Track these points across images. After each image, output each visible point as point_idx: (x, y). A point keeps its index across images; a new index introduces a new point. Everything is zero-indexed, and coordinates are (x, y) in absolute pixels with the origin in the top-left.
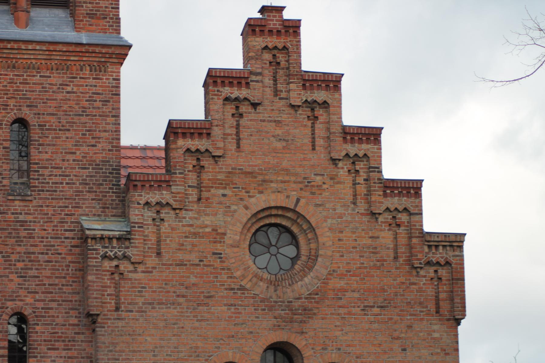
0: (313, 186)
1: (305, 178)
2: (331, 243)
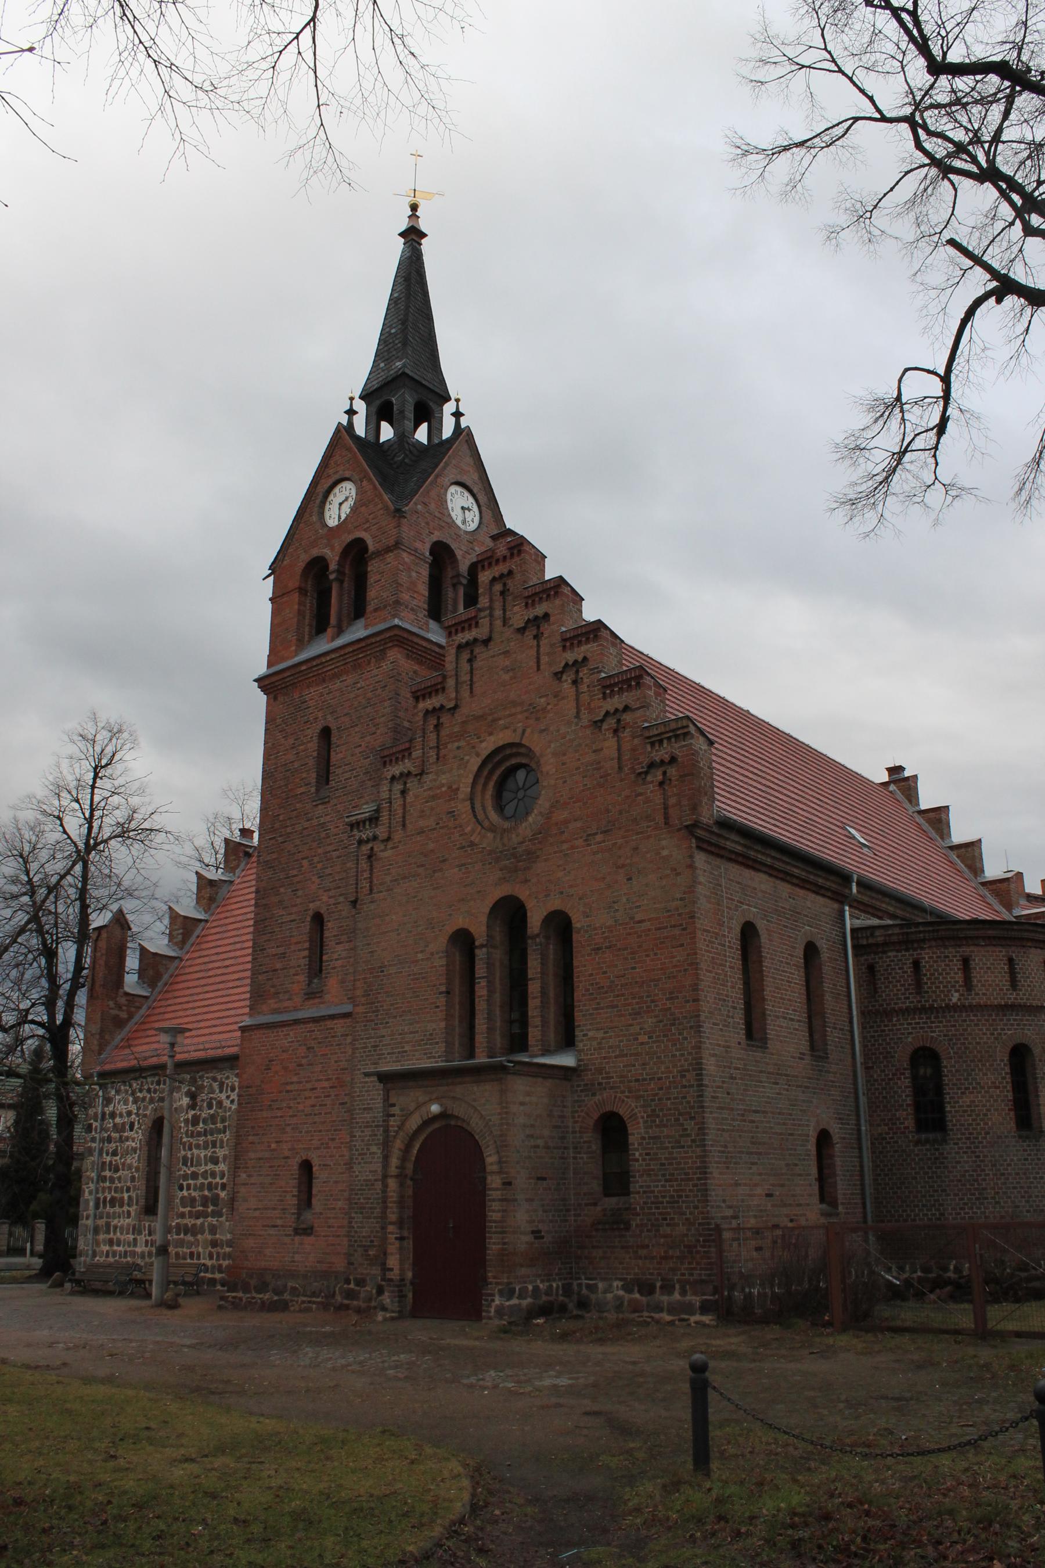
1: (530, 705)
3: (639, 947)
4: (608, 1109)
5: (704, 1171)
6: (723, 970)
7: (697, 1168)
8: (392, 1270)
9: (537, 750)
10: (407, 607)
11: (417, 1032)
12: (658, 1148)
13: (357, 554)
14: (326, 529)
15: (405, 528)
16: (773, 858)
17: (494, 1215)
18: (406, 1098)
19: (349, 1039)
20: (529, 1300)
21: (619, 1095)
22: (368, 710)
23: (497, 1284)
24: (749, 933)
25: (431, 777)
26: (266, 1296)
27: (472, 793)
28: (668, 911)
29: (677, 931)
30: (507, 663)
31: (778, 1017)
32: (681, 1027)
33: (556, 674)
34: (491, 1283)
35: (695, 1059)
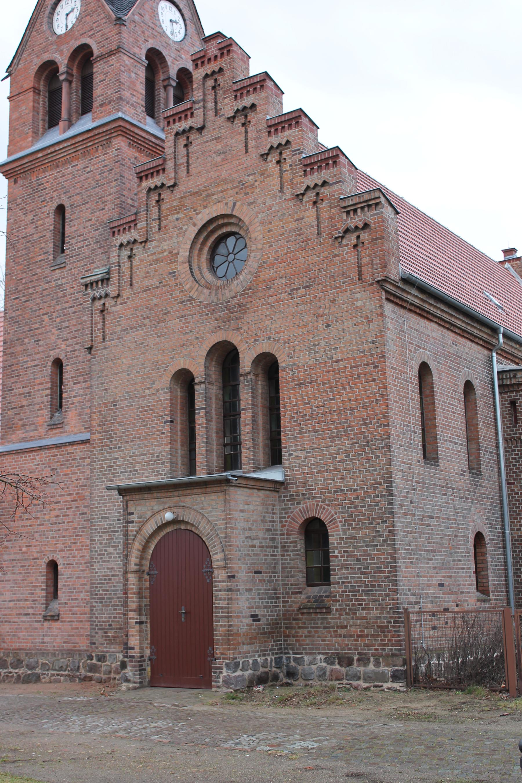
0: (247, 187)
1: (240, 182)
2: (262, 236)
3: (337, 382)
4: (312, 515)
5: (394, 567)
6: (406, 401)
7: (389, 563)
8: (133, 648)
9: (246, 220)
10: (128, 103)
11: (146, 454)
12: (355, 547)
13: (83, 57)
14: (55, 37)
15: (125, 35)
16: (442, 311)
17: (220, 600)
18: (142, 508)
19: (87, 461)
20: (250, 672)
21: (320, 504)
22: (97, 190)
23: (224, 659)
24: (424, 369)
25: (154, 244)
26: (21, 671)
27: (190, 257)
28: (362, 352)
29: (370, 369)
30: (219, 147)
31: (446, 441)
32: (373, 447)
33: (262, 155)
34: (219, 658)
35: (387, 473)
